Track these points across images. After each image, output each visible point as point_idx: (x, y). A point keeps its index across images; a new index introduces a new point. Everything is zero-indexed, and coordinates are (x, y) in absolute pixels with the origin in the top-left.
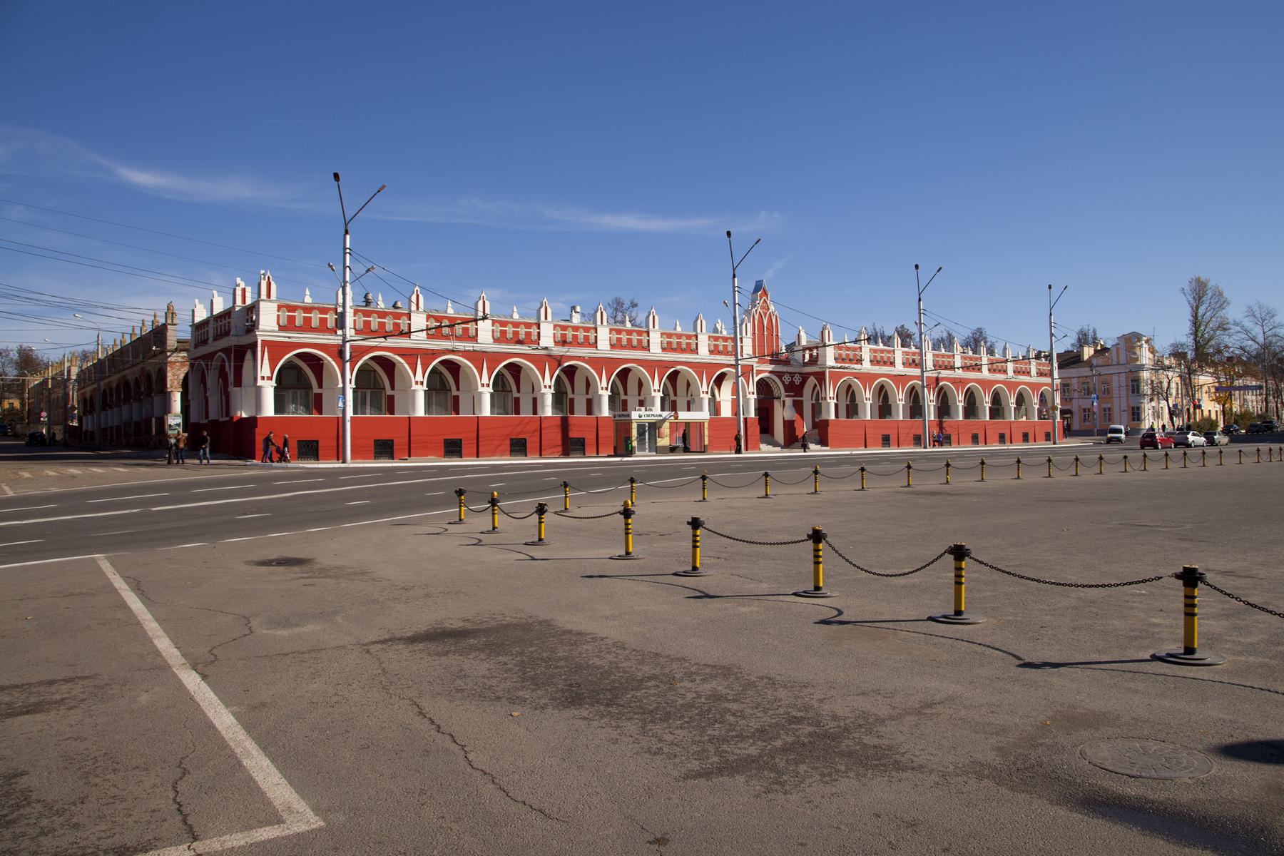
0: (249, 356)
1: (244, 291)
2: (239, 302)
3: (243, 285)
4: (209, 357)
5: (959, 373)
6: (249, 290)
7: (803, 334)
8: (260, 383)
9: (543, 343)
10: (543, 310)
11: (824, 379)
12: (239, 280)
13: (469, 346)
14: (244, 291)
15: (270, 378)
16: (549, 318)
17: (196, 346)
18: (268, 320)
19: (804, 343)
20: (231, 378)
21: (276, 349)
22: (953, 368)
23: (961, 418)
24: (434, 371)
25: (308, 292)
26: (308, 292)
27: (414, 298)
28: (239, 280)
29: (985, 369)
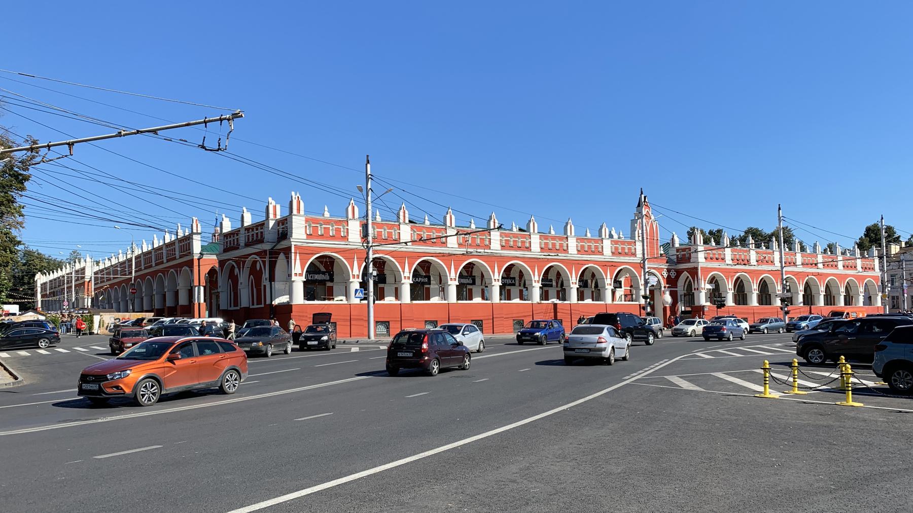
0: (282, 256)
1: (275, 207)
2: (271, 216)
3: (274, 203)
4: (240, 261)
5: (800, 269)
6: (278, 207)
7: (676, 238)
8: (294, 278)
9: (570, 251)
10: (531, 224)
11: (697, 273)
12: (270, 199)
13: (340, 245)
14: (275, 207)
15: (301, 275)
16: (302, 212)
17: (225, 251)
18: (299, 233)
19: (677, 245)
20: (266, 275)
21: (305, 252)
22: (795, 264)
23: (861, 304)
24: (415, 270)
25: (326, 209)
26: (326, 209)
27: (401, 214)
28: (270, 199)
29: (820, 266)
